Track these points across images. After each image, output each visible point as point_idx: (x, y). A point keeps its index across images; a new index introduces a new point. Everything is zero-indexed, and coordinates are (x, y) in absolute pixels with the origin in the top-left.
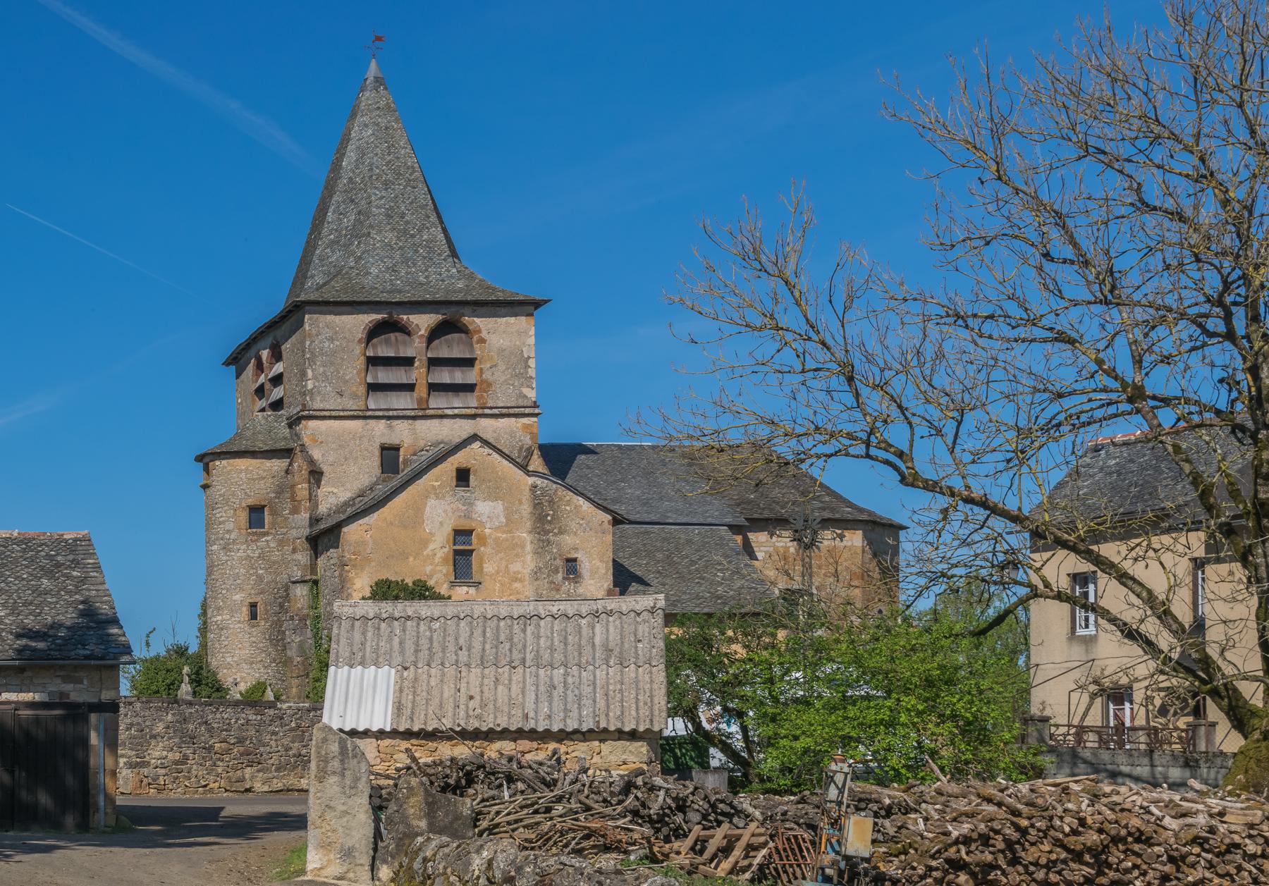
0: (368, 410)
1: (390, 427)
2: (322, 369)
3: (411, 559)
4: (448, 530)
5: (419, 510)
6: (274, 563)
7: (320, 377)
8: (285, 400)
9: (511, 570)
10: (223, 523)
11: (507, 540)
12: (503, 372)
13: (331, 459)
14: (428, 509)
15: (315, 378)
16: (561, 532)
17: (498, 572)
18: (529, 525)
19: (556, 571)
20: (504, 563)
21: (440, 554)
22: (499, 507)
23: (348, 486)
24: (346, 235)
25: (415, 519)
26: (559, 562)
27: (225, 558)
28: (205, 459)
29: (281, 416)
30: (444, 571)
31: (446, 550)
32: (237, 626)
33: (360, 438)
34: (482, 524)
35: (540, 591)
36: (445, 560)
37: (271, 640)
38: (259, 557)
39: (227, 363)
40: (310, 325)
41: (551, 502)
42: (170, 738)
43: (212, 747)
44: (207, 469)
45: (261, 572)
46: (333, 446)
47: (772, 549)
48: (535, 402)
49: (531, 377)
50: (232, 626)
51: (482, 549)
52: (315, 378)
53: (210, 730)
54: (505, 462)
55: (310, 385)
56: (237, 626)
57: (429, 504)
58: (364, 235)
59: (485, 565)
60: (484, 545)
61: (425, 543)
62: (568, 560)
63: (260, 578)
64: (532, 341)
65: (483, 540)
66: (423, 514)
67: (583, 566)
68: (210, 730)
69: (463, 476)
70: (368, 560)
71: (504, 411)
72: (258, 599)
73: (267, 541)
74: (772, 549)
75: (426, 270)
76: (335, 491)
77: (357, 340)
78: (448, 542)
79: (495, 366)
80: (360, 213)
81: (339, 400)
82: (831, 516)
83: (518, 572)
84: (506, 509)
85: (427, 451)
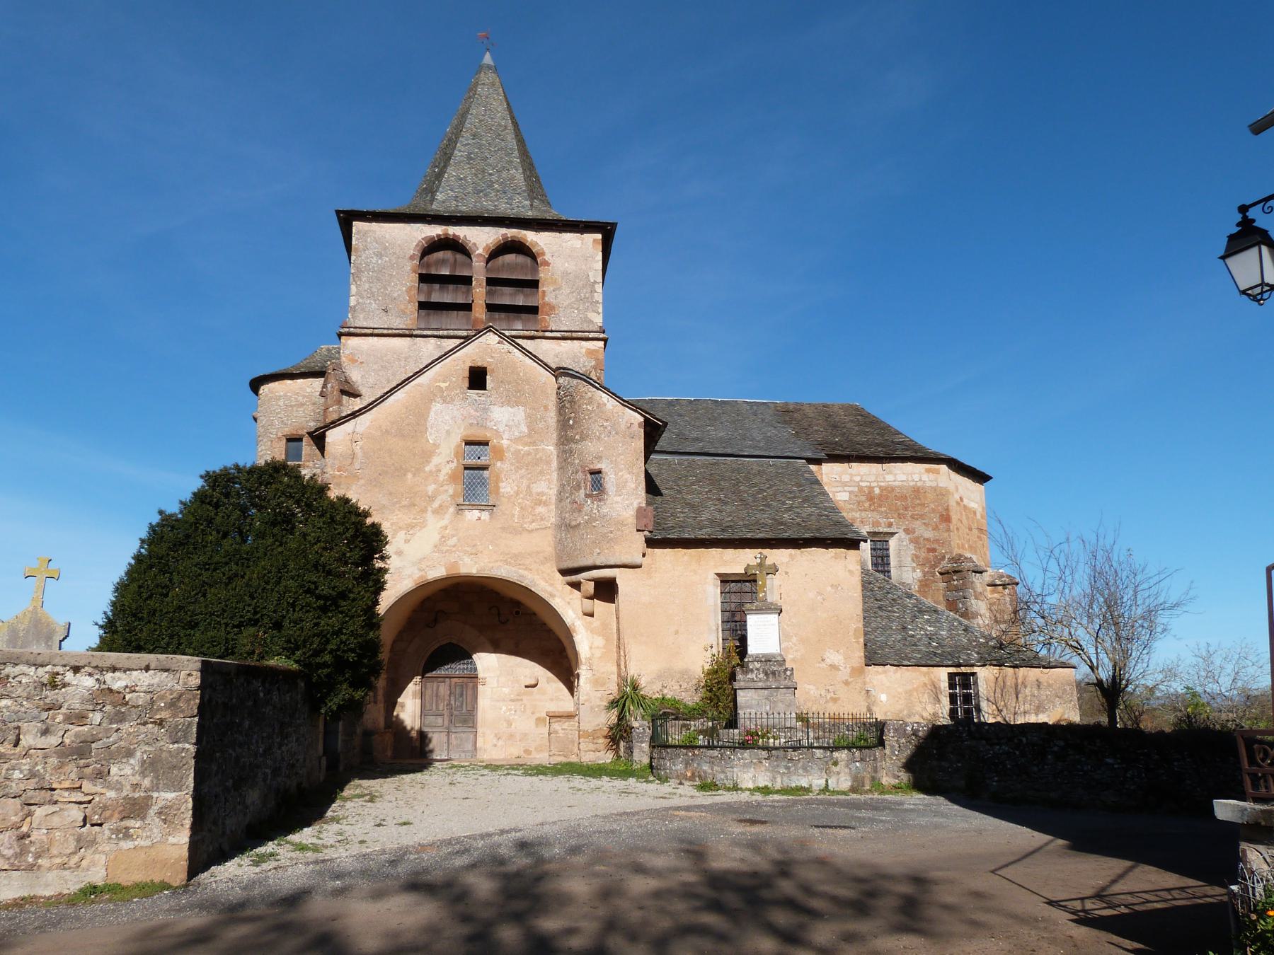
2: (367, 286)
3: (409, 476)
4: (456, 439)
7: (365, 294)
8: (659, 498)
9: (534, 491)
11: (529, 454)
14: (432, 414)
16: (582, 439)
17: (517, 493)
18: (555, 435)
19: (578, 487)
20: (525, 482)
21: (447, 470)
22: (519, 414)
25: (416, 421)
26: (580, 476)
28: (256, 385)
30: (451, 492)
31: (454, 465)
33: (406, 359)
34: (498, 434)
36: (453, 477)
40: (357, 239)
41: (572, 402)
46: (375, 367)
47: (856, 489)
49: (597, 302)
51: (499, 464)
52: (359, 294)
54: (529, 361)
55: (353, 301)
59: (501, 485)
60: (501, 460)
61: (427, 455)
62: (593, 473)
65: (499, 454)
66: (426, 420)
67: (607, 479)
69: (477, 378)
71: (566, 334)
74: (856, 489)
77: (408, 256)
78: (456, 455)
79: (559, 289)
82: (914, 454)
83: (542, 494)
84: (528, 416)
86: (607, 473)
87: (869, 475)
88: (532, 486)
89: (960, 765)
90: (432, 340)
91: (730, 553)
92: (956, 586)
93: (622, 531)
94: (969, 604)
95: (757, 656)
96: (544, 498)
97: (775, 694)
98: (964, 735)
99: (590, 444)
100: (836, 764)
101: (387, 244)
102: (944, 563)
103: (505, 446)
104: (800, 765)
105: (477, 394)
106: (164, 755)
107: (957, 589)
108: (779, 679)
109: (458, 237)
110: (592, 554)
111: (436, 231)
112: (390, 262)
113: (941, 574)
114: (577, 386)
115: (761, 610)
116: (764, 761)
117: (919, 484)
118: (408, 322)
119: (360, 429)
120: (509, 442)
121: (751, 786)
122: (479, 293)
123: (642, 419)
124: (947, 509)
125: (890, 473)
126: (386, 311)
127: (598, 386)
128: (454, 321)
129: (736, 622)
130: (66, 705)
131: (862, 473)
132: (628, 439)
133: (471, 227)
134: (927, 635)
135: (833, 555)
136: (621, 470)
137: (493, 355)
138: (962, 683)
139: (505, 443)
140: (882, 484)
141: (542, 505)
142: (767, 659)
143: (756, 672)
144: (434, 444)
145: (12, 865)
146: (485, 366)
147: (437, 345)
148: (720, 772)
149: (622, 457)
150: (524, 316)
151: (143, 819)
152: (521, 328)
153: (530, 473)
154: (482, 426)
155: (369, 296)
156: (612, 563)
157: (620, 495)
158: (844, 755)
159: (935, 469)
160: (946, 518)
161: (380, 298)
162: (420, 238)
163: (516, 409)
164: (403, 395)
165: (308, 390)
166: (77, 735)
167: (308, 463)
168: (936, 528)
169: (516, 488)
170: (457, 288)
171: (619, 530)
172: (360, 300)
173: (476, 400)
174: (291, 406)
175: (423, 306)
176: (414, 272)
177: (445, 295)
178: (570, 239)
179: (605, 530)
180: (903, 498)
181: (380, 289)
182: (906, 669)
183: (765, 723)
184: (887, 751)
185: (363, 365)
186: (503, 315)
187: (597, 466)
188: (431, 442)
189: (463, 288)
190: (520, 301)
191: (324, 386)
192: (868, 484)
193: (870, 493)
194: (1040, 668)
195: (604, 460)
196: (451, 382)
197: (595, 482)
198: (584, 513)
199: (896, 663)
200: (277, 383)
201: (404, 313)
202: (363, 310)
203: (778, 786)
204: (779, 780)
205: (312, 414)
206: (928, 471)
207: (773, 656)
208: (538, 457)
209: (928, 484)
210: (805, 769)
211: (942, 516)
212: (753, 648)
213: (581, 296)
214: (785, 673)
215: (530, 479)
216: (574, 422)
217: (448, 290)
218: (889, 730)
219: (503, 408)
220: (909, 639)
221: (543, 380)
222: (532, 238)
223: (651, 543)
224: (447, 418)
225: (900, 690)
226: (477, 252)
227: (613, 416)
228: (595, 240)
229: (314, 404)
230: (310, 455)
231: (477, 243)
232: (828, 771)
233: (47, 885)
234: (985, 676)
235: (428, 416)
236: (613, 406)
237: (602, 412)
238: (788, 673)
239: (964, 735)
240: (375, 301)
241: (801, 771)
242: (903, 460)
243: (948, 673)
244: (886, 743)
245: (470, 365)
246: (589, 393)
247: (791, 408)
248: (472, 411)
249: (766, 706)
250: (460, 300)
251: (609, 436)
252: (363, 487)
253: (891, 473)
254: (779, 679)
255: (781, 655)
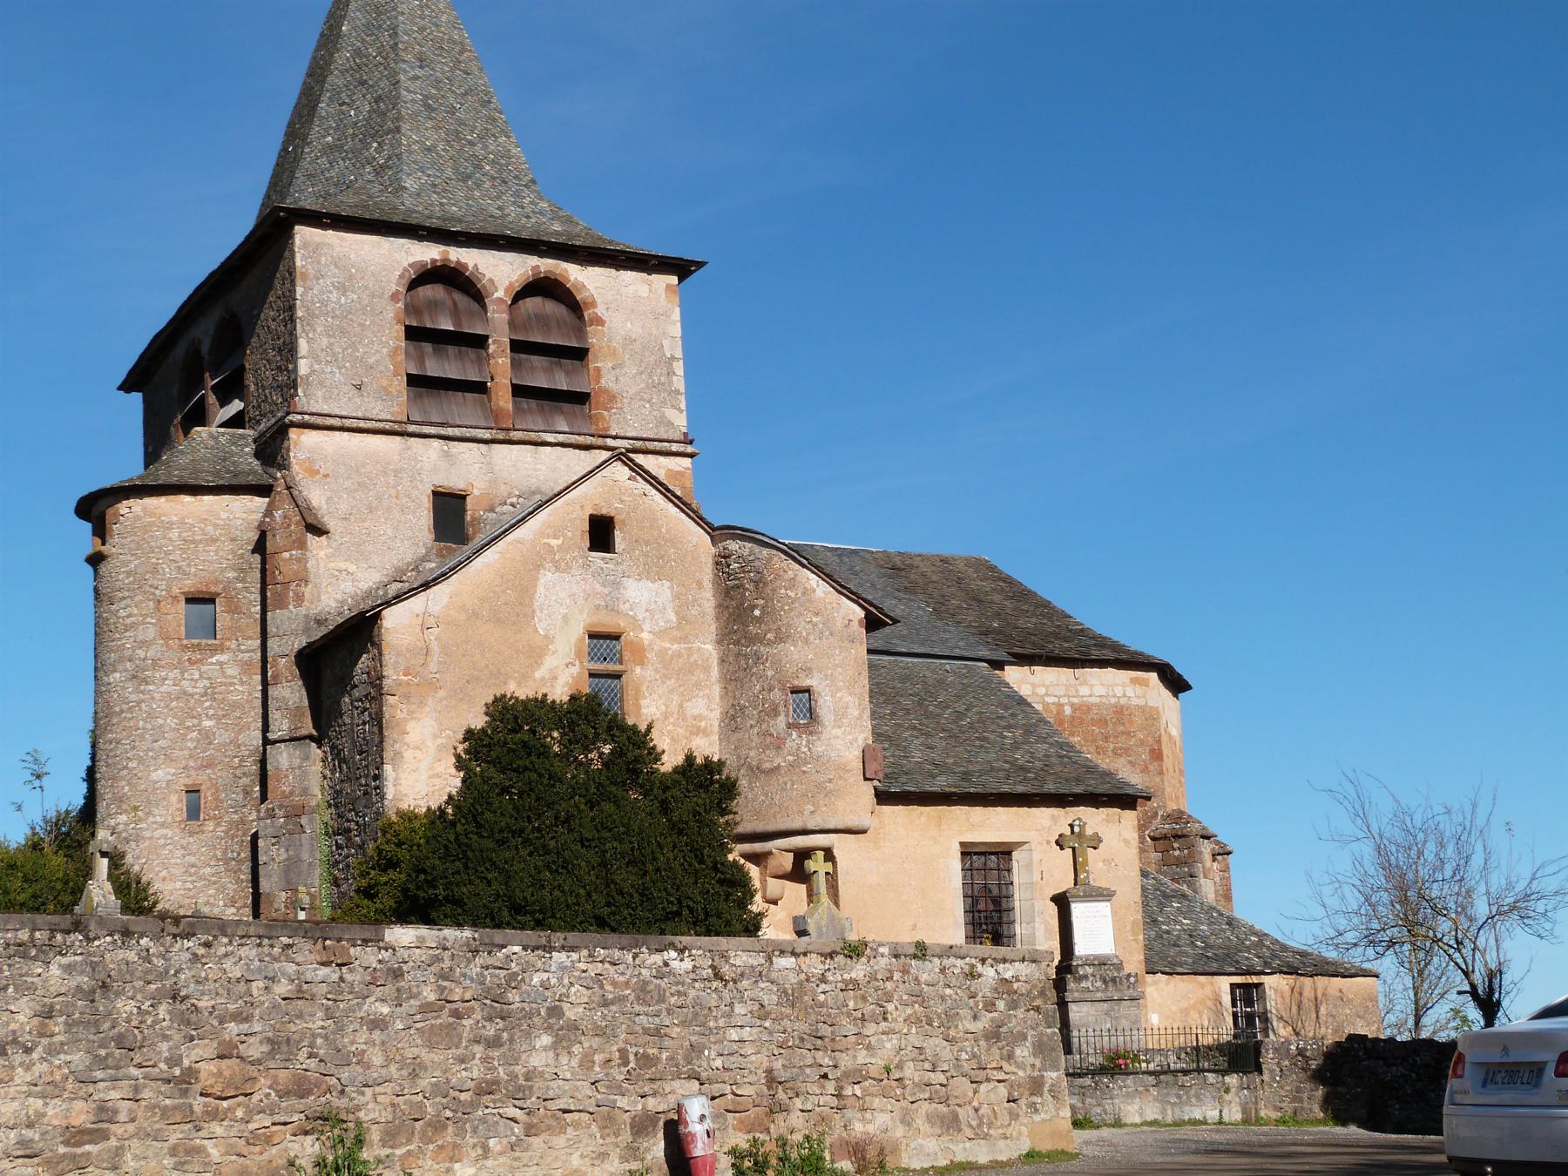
0: (409, 422)
1: (447, 455)
2: (325, 341)
4: (577, 631)
5: (525, 590)
6: (235, 706)
10: (133, 626)
11: (680, 655)
12: (634, 377)
13: (344, 507)
14: (540, 589)
15: (313, 355)
16: (780, 639)
19: (774, 712)
23: (375, 559)
24: (354, 135)
26: (777, 695)
27: (133, 697)
29: (242, 437)
31: (575, 670)
32: (157, 834)
33: (397, 472)
35: (744, 752)
37: (226, 861)
38: (205, 694)
39: (127, 386)
40: (304, 257)
41: (759, 582)
42: (52, 1051)
43: (190, 1075)
44: (101, 531)
45: (207, 723)
46: (348, 484)
48: (685, 434)
49: (677, 391)
50: (147, 834)
51: (638, 670)
52: (313, 355)
53: (190, 1022)
56: (157, 834)
57: (542, 581)
58: (390, 131)
59: (643, 702)
60: (642, 664)
63: (207, 736)
64: (676, 330)
65: (640, 653)
66: (532, 599)
68: (190, 1022)
69: (601, 533)
70: (434, 686)
72: (201, 778)
73: (221, 664)
75: (498, 197)
76: (352, 568)
77: (388, 294)
78: (578, 654)
79: (621, 366)
80: (378, 100)
81: (358, 400)
84: (676, 597)
85: (513, 505)
86: (819, 693)
87: (1058, 685)
88: (685, 705)
89: (1359, 1090)
90: (436, 443)
91: (977, 813)
92: (1177, 858)
93: (846, 780)
94: (1198, 884)
95: (1087, 957)
96: (703, 724)
97: (1117, 1008)
98: (1361, 1054)
99: (792, 648)
100: (1227, 1091)
101: (353, 271)
102: (1157, 822)
103: (646, 642)
104: (1192, 1092)
105: (603, 559)
106: (1045, 1038)
107: (1180, 862)
108: (1122, 988)
109: (465, 266)
110: (801, 812)
111: (430, 253)
112: (359, 303)
113: (1153, 839)
114: (770, 559)
115: (1092, 896)
116: (1151, 1089)
117: (1123, 701)
118: (396, 409)
119: (435, 609)
120: (651, 636)
121: (1137, 1120)
122: (501, 366)
123: (862, 614)
124: (1159, 741)
125: (1084, 683)
126: (359, 388)
127: (805, 562)
128: (462, 408)
129: (980, 912)
130: (980, 995)
131: (1047, 683)
132: (846, 644)
133: (485, 251)
134: (1185, 930)
135: (1104, 817)
136: (839, 690)
137: (623, 498)
138: (1247, 994)
139: (646, 636)
140: (1075, 700)
141: (701, 735)
142: (1101, 962)
143: (1091, 978)
144: (546, 637)
145: (977, 1134)
146: (612, 515)
147: (443, 450)
148: (1094, 1106)
149: (840, 670)
150: (566, 406)
151: (1041, 1096)
152: (567, 430)
153: (683, 685)
154: (612, 610)
155: (329, 359)
156: (831, 826)
157: (840, 727)
158: (1234, 1081)
159: (1143, 679)
160: (1157, 755)
161: (348, 364)
162: (406, 264)
163: (657, 585)
164: (497, 556)
165: (224, 515)
166: (992, 1020)
167: (228, 643)
168: (1145, 770)
169: (664, 708)
170: (460, 352)
171: (841, 778)
172: (316, 367)
173: (602, 569)
174: (193, 542)
175: (414, 381)
176: (399, 322)
177: (446, 365)
178: (631, 280)
179: (821, 778)
180: (1102, 722)
181: (346, 349)
182: (1180, 979)
183: (1106, 1045)
184: (1266, 1077)
185: (328, 480)
186: (533, 403)
187: (806, 682)
188: (541, 632)
189: (471, 353)
190: (562, 383)
191: (268, 512)
192: (1056, 700)
193: (1058, 713)
194: (1337, 976)
195: (816, 674)
196: (565, 537)
197: (798, 706)
198: (786, 751)
199: (1167, 969)
200: (163, 499)
201: (388, 393)
202: (321, 383)
203: (1169, 1119)
204: (1170, 1112)
205: (230, 557)
206: (1134, 681)
207: (1108, 957)
208: (692, 660)
209: (1135, 701)
210: (1198, 1097)
211: (1152, 751)
212: (1081, 948)
213: (653, 381)
214: (1128, 980)
215: (682, 694)
216: (763, 613)
217: (448, 358)
218: (1267, 1050)
219: (641, 583)
220: (1165, 936)
221: (695, 540)
222: (584, 278)
223: (883, 797)
224: (562, 595)
225: (1174, 1008)
226: (496, 295)
227: (826, 609)
228: (669, 287)
229: (233, 540)
230: (230, 628)
231: (496, 279)
232: (1220, 1100)
233: (1001, 1152)
234: (1275, 986)
235: (535, 591)
236: (824, 592)
237: (810, 601)
238: (1132, 980)
239: (1361, 1054)
240: (340, 368)
241: (1193, 1100)
242: (1102, 663)
243: (1231, 984)
244: (1264, 1066)
245: (591, 512)
246: (790, 572)
247: (897, 560)
248: (598, 586)
249: (1105, 1023)
250: (473, 376)
251: (820, 638)
252: (444, 702)
253: (1086, 684)
254: (1122, 988)
255: (1117, 957)
